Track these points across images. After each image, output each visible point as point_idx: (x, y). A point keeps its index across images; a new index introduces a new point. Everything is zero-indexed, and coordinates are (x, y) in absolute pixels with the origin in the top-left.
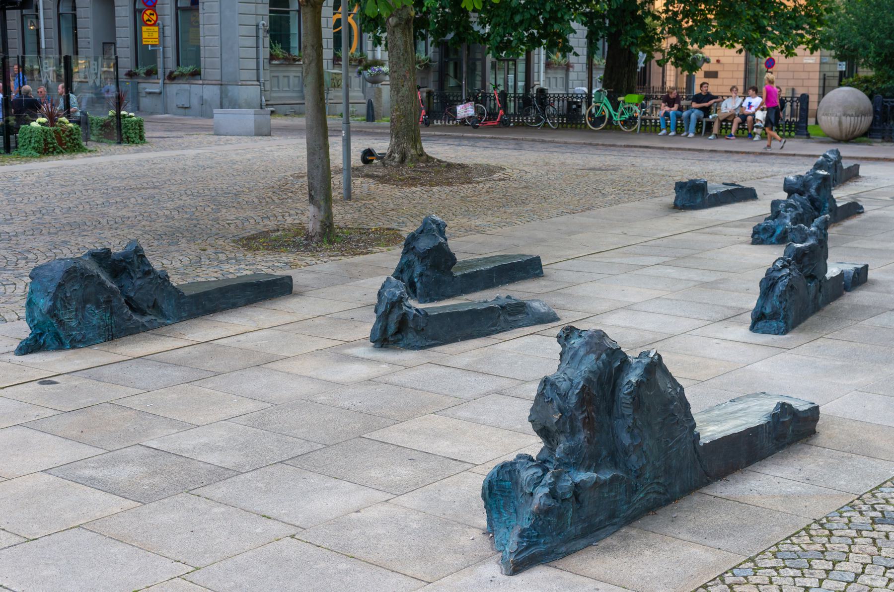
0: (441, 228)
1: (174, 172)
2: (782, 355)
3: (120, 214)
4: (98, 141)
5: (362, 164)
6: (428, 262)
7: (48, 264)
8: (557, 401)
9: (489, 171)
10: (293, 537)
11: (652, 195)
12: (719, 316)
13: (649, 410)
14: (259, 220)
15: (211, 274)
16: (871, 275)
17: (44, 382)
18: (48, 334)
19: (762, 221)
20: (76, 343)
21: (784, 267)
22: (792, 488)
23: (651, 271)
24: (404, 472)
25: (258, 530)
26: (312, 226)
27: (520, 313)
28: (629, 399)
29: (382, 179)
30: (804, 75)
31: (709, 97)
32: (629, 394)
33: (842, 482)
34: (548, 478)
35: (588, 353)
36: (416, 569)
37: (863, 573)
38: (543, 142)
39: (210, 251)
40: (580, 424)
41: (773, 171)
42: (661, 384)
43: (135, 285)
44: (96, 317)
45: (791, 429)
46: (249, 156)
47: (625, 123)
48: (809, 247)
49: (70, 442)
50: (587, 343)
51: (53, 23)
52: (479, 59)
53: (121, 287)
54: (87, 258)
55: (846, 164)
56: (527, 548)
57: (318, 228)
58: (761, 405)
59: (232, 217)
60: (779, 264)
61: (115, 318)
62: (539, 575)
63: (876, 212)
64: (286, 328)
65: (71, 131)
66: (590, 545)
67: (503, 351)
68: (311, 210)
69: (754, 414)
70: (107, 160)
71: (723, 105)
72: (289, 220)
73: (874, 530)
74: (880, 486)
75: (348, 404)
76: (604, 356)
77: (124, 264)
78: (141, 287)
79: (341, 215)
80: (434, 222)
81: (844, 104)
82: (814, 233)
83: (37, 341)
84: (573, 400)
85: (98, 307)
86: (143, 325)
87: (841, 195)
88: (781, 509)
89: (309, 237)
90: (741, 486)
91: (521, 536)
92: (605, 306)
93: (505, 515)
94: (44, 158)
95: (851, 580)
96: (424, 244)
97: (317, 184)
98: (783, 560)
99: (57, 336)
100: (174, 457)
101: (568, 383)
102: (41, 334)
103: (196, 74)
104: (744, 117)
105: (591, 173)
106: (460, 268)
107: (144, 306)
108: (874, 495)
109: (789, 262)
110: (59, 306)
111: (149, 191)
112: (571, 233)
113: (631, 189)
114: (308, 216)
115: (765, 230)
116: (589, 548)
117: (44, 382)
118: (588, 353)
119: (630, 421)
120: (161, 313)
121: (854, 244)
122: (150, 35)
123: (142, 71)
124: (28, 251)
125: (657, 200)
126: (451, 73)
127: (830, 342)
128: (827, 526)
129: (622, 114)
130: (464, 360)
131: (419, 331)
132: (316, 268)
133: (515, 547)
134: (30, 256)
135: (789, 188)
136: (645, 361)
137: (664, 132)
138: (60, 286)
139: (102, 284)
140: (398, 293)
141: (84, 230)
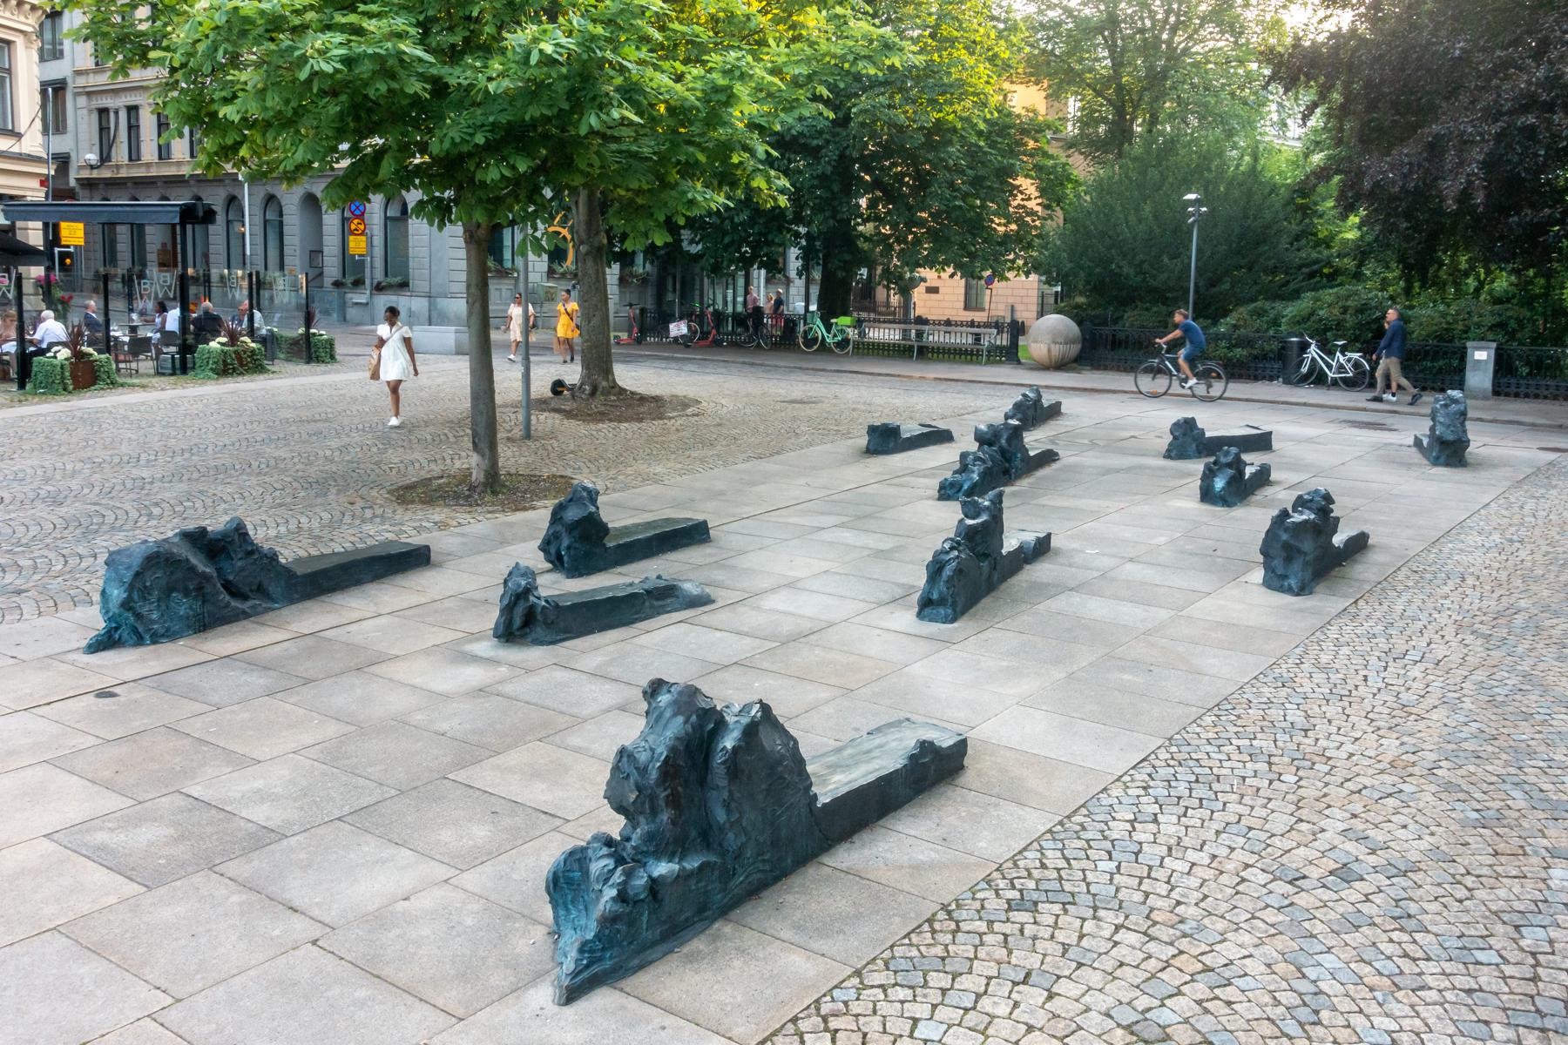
0: (592, 496)
1: (354, 400)
2: (945, 652)
3: (276, 454)
4: (287, 360)
6: (576, 533)
7: (127, 549)
8: (635, 776)
9: (684, 404)
10: (314, 943)
11: (847, 435)
12: (885, 597)
13: (749, 777)
14: (425, 463)
15: (347, 540)
16: (1054, 543)
17: (104, 694)
19: (948, 475)
20: (156, 639)
21: (952, 548)
22: (924, 853)
23: (826, 536)
24: (480, 833)
25: (277, 932)
26: (477, 476)
27: (669, 596)
28: (722, 771)
29: (569, 414)
30: (1024, 292)
32: (724, 763)
33: (983, 844)
34: (618, 877)
36: (451, 997)
37: (974, 1008)
38: (753, 364)
39: (360, 503)
40: (662, 803)
41: (976, 403)
42: (767, 743)
43: (236, 567)
44: (183, 606)
45: (934, 770)
46: (440, 381)
47: (838, 345)
48: (983, 524)
49: (97, 788)
51: (259, 230)
53: (219, 570)
54: (176, 540)
55: (1046, 402)
56: (587, 967)
57: (482, 478)
58: (901, 740)
59: (396, 460)
60: (947, 546)
61: (209, 607)
62: (602, 1000)
63: (1072, 460)
64: (408, 613)
65: (253, 351)
66: (671, 951)
67: (642, 647)
68: (475, 459)
69: (889, 758)
70: (289, 384)
72: (458, 464)
73: (1008, 920)
74: (1025, 849)
75: (445, 726)
76: (694, 718)
78: (242, 569)
79: (510, 458)
80: (585, 489)
81: (1051, 330)
82: (987, 508)
85: (186, 595)
86: (244, 612)
87: (1035, 440)
88: (907, 887)
89: (472, 488)
90: (866, 852)
91: (581, 951)
92: (765, 584)
93: (574, 913)
94: (222, 380)
95: (970, 1005)
96: (573, 514)
97: (481, 431)
98: (895, 972)
99: (135, 630)
100: (213, 811)
101: (649, 753)
102: (116, 629)
103: (404, 285)
105: (790, 406)
106: (617, 537)
107: (246, 590)
108: (1016, 865)
109: (958, 543)
110: (136, 597)
111: (320, 425)
112: (754, 484)
113: (828, 428)
114: (470, 462)
115: (952, 485)
116: (669, 957)
117: (104, 694)
118: (675, 715)
119: (725, 795)
121: (1043, 501)
122: (357, 245)
123: (349, 280)
124: (157, 504)
125: (850, 442)
127: (1000, 633)
128: (955, 915)
130: (592, 661)
131: (549, 625)
132: (467, 529)
133: (572, 966)
134: (156, 511)
135: (981, 438)
136: (745, 720)
138: (137, 574)
139: (192, 569)
140: (523, 583)
141: (231, 476)
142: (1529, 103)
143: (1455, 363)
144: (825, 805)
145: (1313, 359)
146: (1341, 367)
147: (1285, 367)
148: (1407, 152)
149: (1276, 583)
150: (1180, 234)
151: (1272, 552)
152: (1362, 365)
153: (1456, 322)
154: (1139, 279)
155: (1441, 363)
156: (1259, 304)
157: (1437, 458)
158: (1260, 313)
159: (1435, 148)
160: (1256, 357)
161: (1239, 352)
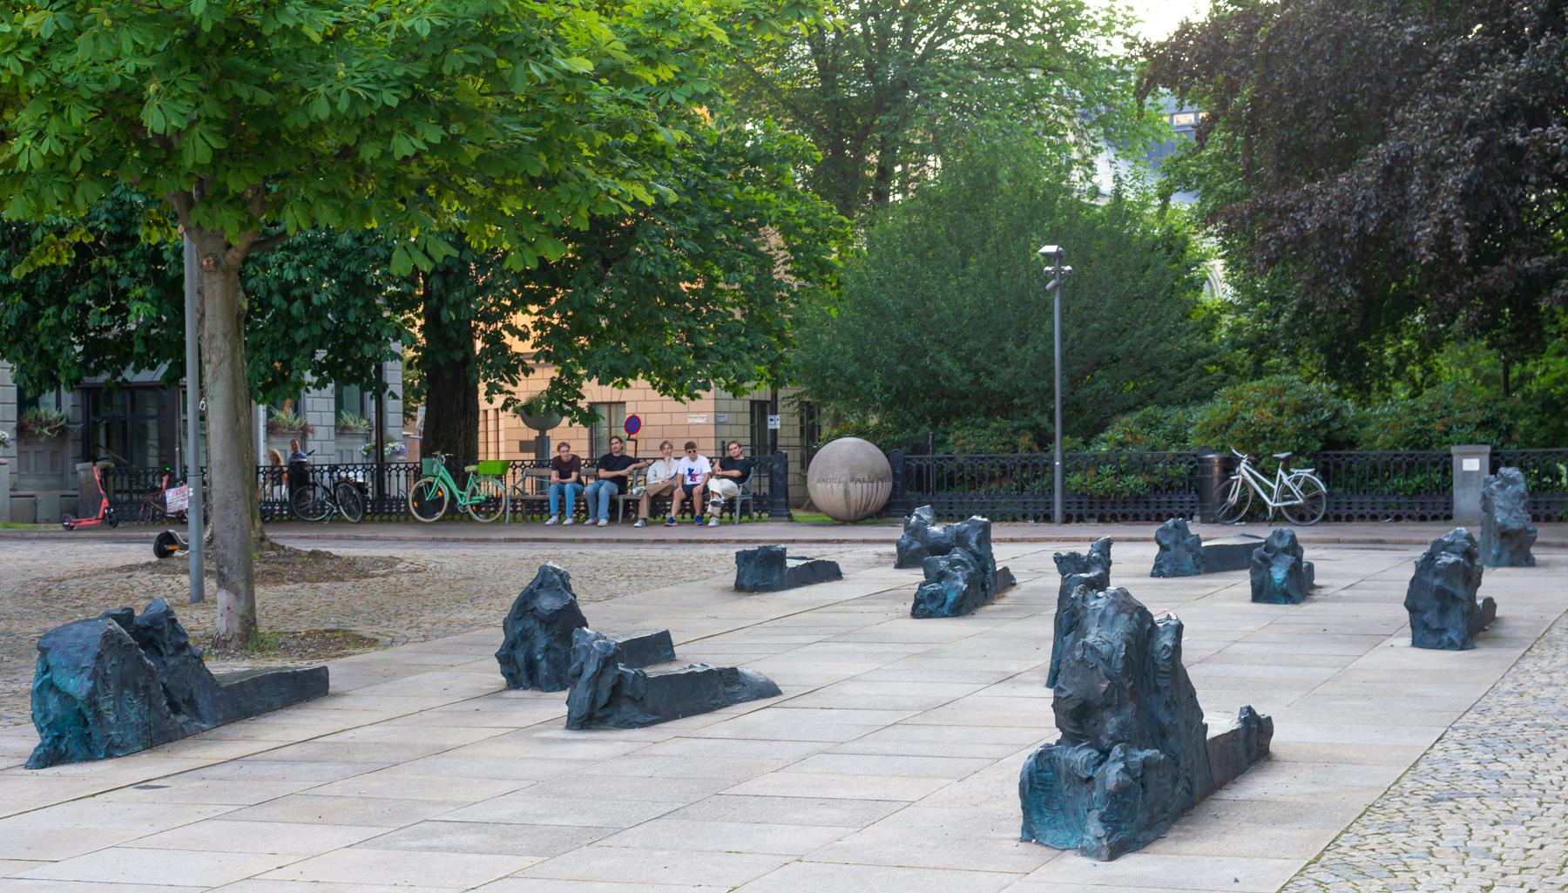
5: (155, 559)
18: (71, 737)
20: (112, 750)
31: (625, 461)
35: (1118, 613)
50: (1113, 602)
52: (152, 417)
71: (650, 472)
77: (151, 633)
80: (556, 571)
83: (56, 748)
84: (1120, 665)
102: (60, 737)
104: (688, 490)
118: (1118, 613)
120: (196, 713)
126: (102, 442)
129: (474, 493)
131: (638, 701)
137: (554, 519)
142: (1509, 111)
143: (1437, 478)
144: (1215, 739)
145: (1245, 483)
146: (1287, 490)
147: (1202, 500)
148: (1358, 181)
149: (1431, 639)
150: (1032, 309)
151: (1420, 605)
152: (1316, 487)
153: (1431, 420)
154: (968, 378)
155: (1418, 479)
156: (1150, 410)
157: (1499, 557)
158: (1152, 424)
159: (1394, 175)
160: (1156, 488)
161: (1134, 481)
